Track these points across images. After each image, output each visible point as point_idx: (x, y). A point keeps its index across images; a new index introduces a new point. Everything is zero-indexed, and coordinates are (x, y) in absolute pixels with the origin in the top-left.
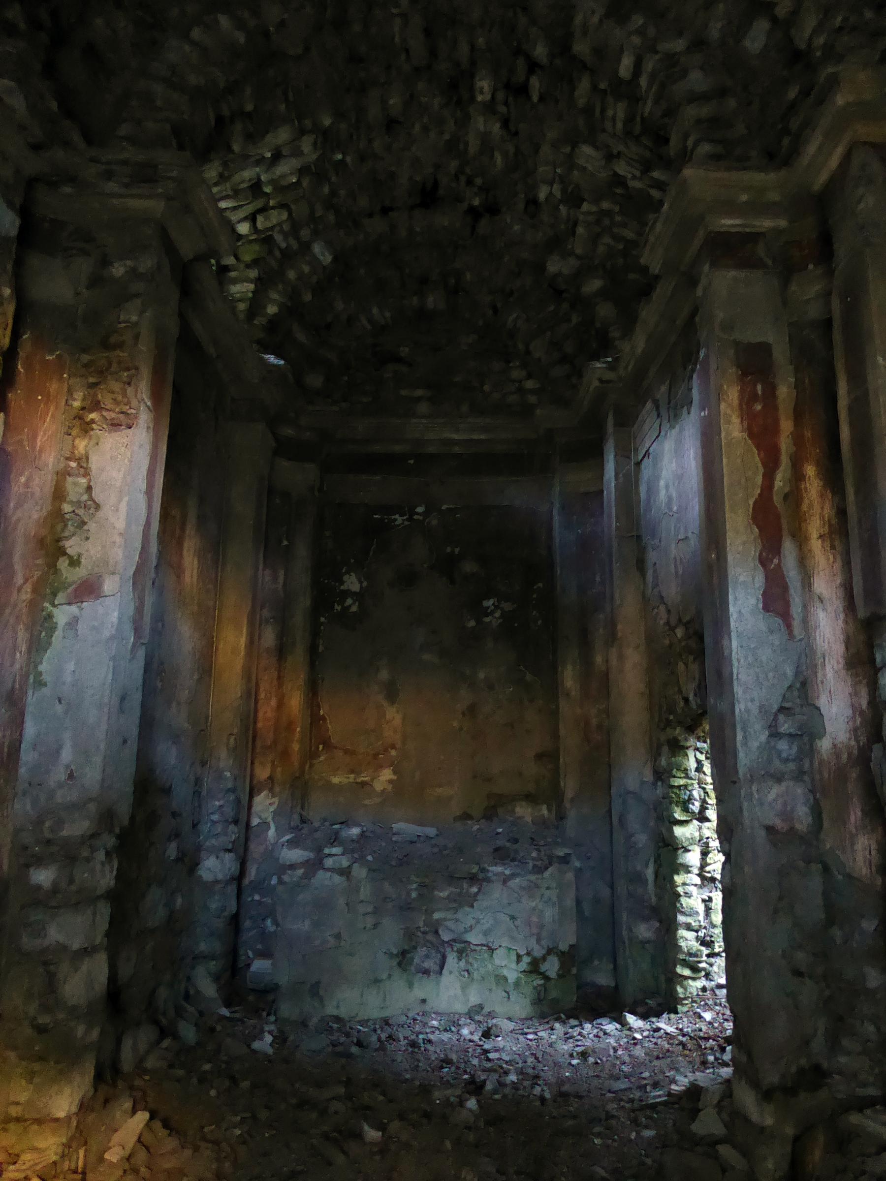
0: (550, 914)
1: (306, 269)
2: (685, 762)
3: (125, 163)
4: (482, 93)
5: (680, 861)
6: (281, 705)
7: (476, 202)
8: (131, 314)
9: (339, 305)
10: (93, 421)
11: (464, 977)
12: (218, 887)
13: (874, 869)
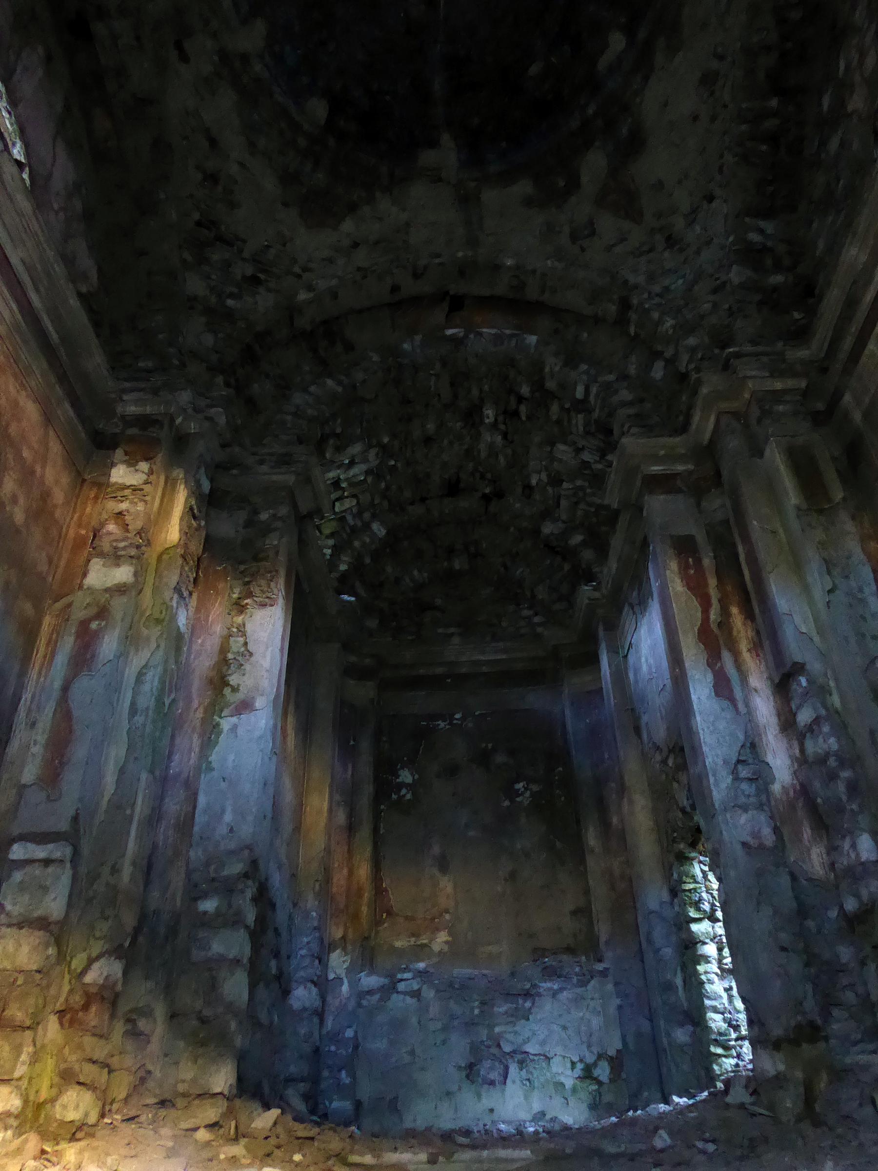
0: (596, 1022)
1: (368, 540)
2: (692, 870)
3: (272, 454)
4: (488, 418)
5: (700, 952)
6: (351, 873)
7: (487, 491)
8: (273, 540)
9: (389, 569)
10: (247, 604)
11: (525, 1085)
12: (305, 1015)
13: (827, 869)
